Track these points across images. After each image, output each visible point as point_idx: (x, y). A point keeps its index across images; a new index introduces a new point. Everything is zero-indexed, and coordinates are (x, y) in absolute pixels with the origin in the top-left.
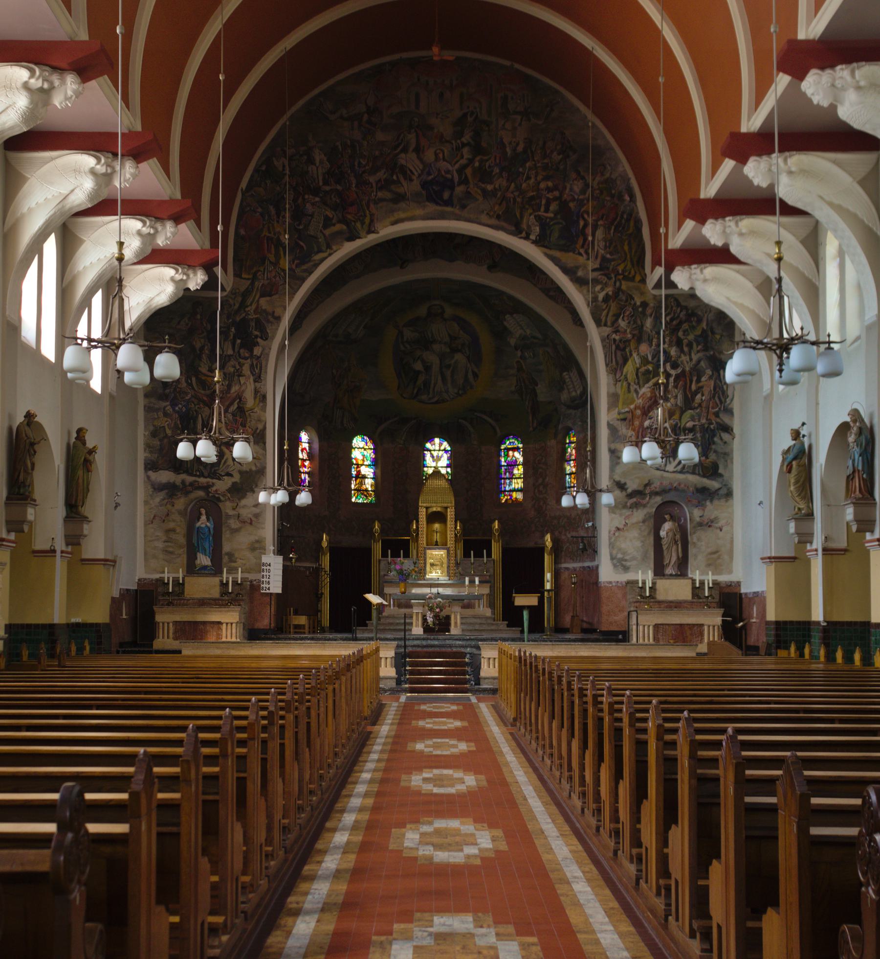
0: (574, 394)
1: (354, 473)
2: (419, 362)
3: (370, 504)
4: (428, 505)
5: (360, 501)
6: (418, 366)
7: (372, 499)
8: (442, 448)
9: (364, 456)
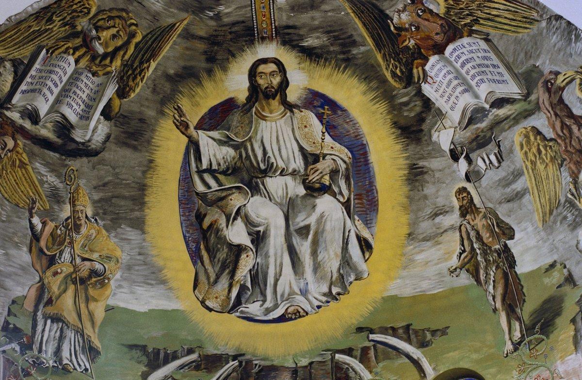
2: (239, 224)
6: (237, 234)
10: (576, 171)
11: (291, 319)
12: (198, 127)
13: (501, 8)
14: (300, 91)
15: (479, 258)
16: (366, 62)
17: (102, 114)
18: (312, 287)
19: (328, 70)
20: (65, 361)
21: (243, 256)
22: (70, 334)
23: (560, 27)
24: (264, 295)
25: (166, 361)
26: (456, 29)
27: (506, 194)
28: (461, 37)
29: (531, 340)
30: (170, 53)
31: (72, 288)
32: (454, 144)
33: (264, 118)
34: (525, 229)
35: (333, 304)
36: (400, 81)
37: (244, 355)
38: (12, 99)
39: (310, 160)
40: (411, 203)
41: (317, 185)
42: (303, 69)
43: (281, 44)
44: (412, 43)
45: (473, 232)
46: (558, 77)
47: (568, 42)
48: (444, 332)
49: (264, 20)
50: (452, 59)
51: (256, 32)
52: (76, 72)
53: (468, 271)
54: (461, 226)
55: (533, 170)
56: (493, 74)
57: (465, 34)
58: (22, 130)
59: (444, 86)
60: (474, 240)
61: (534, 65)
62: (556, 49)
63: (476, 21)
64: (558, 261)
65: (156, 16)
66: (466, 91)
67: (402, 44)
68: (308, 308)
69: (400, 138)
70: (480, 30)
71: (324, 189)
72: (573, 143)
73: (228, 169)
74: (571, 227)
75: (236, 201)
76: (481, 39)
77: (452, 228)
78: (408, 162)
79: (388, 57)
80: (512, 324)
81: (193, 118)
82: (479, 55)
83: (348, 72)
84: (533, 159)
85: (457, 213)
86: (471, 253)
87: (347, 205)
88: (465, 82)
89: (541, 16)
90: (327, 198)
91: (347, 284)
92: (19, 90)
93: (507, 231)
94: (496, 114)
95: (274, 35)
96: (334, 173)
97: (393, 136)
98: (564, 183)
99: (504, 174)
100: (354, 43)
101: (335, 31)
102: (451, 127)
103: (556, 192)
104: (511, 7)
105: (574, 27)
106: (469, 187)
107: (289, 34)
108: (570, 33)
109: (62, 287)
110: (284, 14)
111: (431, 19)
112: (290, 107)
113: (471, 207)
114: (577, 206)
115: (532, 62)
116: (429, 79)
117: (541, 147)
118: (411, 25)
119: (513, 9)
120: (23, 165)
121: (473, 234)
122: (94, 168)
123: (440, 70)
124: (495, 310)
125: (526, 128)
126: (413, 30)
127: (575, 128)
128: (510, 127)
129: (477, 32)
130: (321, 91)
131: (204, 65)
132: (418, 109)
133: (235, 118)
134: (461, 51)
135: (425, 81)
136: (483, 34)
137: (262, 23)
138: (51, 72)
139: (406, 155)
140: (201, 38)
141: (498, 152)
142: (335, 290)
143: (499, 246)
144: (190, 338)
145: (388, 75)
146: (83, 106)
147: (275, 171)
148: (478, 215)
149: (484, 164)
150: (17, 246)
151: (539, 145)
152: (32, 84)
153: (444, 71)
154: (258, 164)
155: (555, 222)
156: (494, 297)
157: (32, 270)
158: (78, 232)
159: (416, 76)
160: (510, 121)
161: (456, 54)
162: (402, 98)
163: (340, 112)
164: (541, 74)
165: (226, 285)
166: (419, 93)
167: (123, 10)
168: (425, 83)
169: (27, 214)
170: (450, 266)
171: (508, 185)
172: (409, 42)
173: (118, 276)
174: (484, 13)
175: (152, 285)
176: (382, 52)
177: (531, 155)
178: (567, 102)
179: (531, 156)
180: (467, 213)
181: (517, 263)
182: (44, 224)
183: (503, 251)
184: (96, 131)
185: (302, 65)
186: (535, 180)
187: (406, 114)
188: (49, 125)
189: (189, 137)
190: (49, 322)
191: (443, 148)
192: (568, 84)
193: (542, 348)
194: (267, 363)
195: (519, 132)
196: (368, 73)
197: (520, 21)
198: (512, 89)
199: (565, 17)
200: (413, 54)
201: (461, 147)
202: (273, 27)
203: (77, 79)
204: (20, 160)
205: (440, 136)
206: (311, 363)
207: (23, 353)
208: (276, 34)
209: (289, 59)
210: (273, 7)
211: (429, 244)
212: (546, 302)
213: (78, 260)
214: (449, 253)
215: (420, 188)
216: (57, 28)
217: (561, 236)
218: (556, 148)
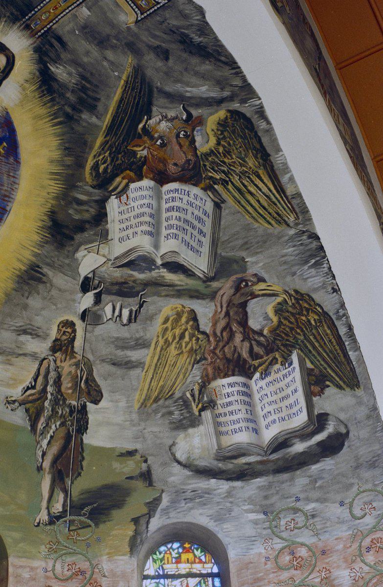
0: (243, 438)
10: (211, 376)
13: (263, 190)
15: (46, 404)
16: (83, 134)
19: (43, 111)
23: (307, 245)
27: (115, 355)
28: (196, 185)
29: (74, 521)
32: (94, 274)
34: (117, 401)
36: (95, 177)
40: (6, 302)
42: (24, 90)
43: (34, 48)
44: (142, 153)
45: (54, 373)
46: (260, 283)
47: (302, 262)
49: (50, 12)
50: (165, 197)
51: (30, 15)
53: (27, 410)
54: (45, 359)
55: (162, 349)
56: (193, 239)
57: (202, 185)
59: (132, 214)
60: (51, 382)
61: (243, 259)
62: (283, 259)
63: (224, 183)
64: (140, 452)
66: (150, 233)
67: (133, 147)
69: (45, 230)
70: (220, 192)
72: (226, 349)
74: (173, 426)
76: (212, 200)
77: (34, 356)
78: (34, 259)
79: (107, 146)
80: (55, 494)
82: (196, 212)
83: (58, 129)
84: (170, 339)
86: (40, 394)
88: (157, 225)
89: (297, 224)
93: (93, 393)
94: (162, 274)
95: (39, 34)
97: (40, 224)
98: (189, 380)
101: (89, 82)
102: (104, 256)
103: (174, 383)
104: (275, 196)
105: (323, 254)
106: (80, 326)
107: (52, 46)
108: (312, 256)
110: (71, 25)
111: (185, 148)
113: (67, 347)
114: (192, 408)
115: (243, 254)
116: (124, 198)
117: (187, 334)
118: (161, 137)
119: (274, 199)
121: (53, 375)
123: (144, 197)
124: (40, 469)
125: (183, 306)
126: (158, 143)
127: (238, 337)
128: (167, 296)
129: (215, 192)
130: (16, 124)
132: (87, 216)
134: (181, 196)
135: (119, 196)
136: (219, 197)
137: (45, 13)
139: (38, 251)
141: (136, 311)
143: (76, 404)
145: (90, 163)
148: (70, 359)
149: (111, 313)
151: (186, 330)
153: (146, 201)
155: (156, 411)
156: (44, 454)
159: (115, 184)
160: (172, 291)
161: (174, 195)
162: (82, 194)
163: (11, 160)
164: (244, 269)
166: (102, 203)
168: (116, 198)
170: (10, 394)
171: (123, 348)
172: (142, 150)
174: (241, 182)
176: (108, 138)
177: (170, 335)
178: (249, 309)
180: (60, 350)
181: (88, 431)
183: (78, 411)
185: (27, 85)
186: (158, 360)
191: (80, 270)
192: (264, 295)
193: (86, 534)
195: (174, 306)
196: (74, 147)
197: (270, 214)
198: (201, 264)
199: (322, 240)
200: (133, 163)
201: (100, 282)
202: (48, 26)
205: (88, 256)
208: (42, 34)
209: (24, 67)
210: (73, 9)
214: (15, 380)
215: (26, 294)
217: (156, 429)
218: (203, 343)
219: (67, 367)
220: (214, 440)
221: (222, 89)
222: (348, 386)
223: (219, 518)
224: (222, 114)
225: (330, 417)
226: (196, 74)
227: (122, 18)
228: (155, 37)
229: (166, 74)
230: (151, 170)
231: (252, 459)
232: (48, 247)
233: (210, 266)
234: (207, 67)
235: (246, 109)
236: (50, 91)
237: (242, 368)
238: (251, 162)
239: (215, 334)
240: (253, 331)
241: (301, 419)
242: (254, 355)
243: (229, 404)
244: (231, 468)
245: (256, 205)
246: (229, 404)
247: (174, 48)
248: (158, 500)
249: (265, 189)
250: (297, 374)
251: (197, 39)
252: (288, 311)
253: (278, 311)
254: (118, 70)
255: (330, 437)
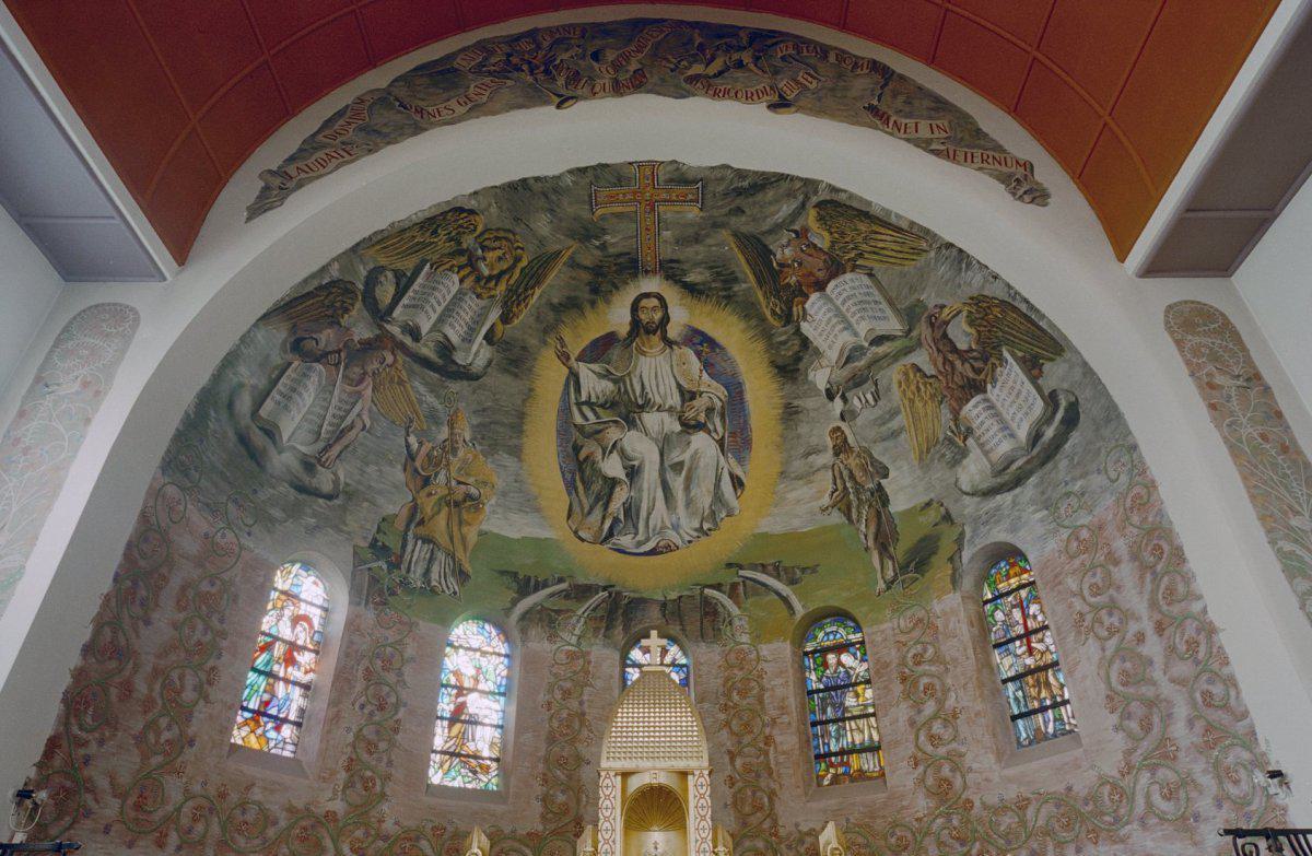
0: (1005, 447)
1: (445, 706)
3: (483, 794)
4: (628, 765)
5: (456, 784)
6: (613, 467)
7: (491, 781)
8: (668, 660)
9: (479, 669)
10: (957, 408)
11: (662, 553)
12: (579, 359)
14: (680, 328)
17: (485, 338)
18: (684, 522)
20: (434, 583)
21: (618, 489)
22: (441, 556)
24: (636, 527)
25: (536, 589)
26: (839, 264)
28: (844, 273)
30: (555, 283)
31: (445, 510)
33: (644, 353)
35: (703, 538)
37: (613, 586)
38: (392, 312)
39: (687, 396)
41: (693, 423)
48: (814, 570)
52: (460, 291)
57: (848, 269)
58: (402, 346)
63: (861, 255)
65: (542, 241)
66: (845, 329)
68: (679, 543)
71: (700, 427)
72: (955, 379)
73: (606, 402)
75: (613, 434)
77: (825, 467)
81: (575, 349)
85: (831, 452)
87: (721, 442)
88: (845, 320)
89: (931, 245)
90: (702, 435)
91: (718, 520)
92: (401, 304)
96: (710, 410)
99: (880, 412)
100: (736, 280)
106: (844, 426)
108: (960, 262)
109: (436, 509)
112: (670, 343)
115: (916, 296)
116: (808, 317)
118: (794, 261)
120: (401, 382)
121: (845, 473)
122: (474, 392)
123: (820, 309)
124: (867, 549)
127: (958, 363)
129: (860, 267)
131: (587, 296)
132: (796, 348)
133: (615, 353)
135: (805, 319)
138: (434, 289)
140: (586, 268)
142: (706, 526)
144: (561, 567)
145: (768, 313)
146: (465, 328)
147: (652, 407)
150: (391, 463)
151: (918, 382)
152: (414, 299)
154: (636, 399)
155: (932, 460)
156: (866, 536)
157: (407, 489)
158: (455, 455)
159: (795, 314)
163: (718, 350)
164: (926, 308)
165: (600, 517)
166: (798, 331)
167: (509, 231)
169: (403, 432)
173: (493, 502)
175: (527, 512)
178: (950, 336)
179: (909, 394)
182: (421, 444)
184: (477, 354)
185: (684, 301)
187: (783, 353)
188: (431, 344)
189: (570, 368)
190: (419, 542)
193: (917, 586)
194: (637, 595)
196: (749, 311)
198: (893, 325)
203: (461, 299)
204: (399, 377)
206: (680, 597)
207: (390, 572)
209: (671, 294)
211: (801, 482)
212: (922, 540)
213: (453, 483)
216: (442, 244)
218: (936, 385)
219: (853, 462)
220: (985, 460)
221: (795, 197)
222: (1056, 354)
223: (1013, 530)
224: (813, 213)
225: (1059, 392)
226: (770, 203)
227: (690, 216)
228: (721, 207)
229: (754, 220)
230: (808, 286)
231: (1019, 463)
232: (787, 387)
233: (901, 322)
234: (770, 194)
235: (824, 196)
236: (701, 293)
237: (975, 387)
238: (863, 227)
239: (940, 372)
240: (965, 351)
241: (1039, 405)
242: (978, 371)
243: (982, 423)
244: (1008, 479)
245: (894, 254)
246: (982, 423)
247: (739, 201)
248: (962, 534)
249: (888, 238)
250: (1016, 368)
251: (745, 184)
252: (977, 319)
253: (971, 323)
254: (724, 243)
255: (1066, 410)
